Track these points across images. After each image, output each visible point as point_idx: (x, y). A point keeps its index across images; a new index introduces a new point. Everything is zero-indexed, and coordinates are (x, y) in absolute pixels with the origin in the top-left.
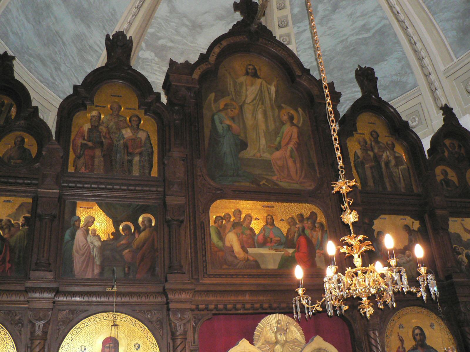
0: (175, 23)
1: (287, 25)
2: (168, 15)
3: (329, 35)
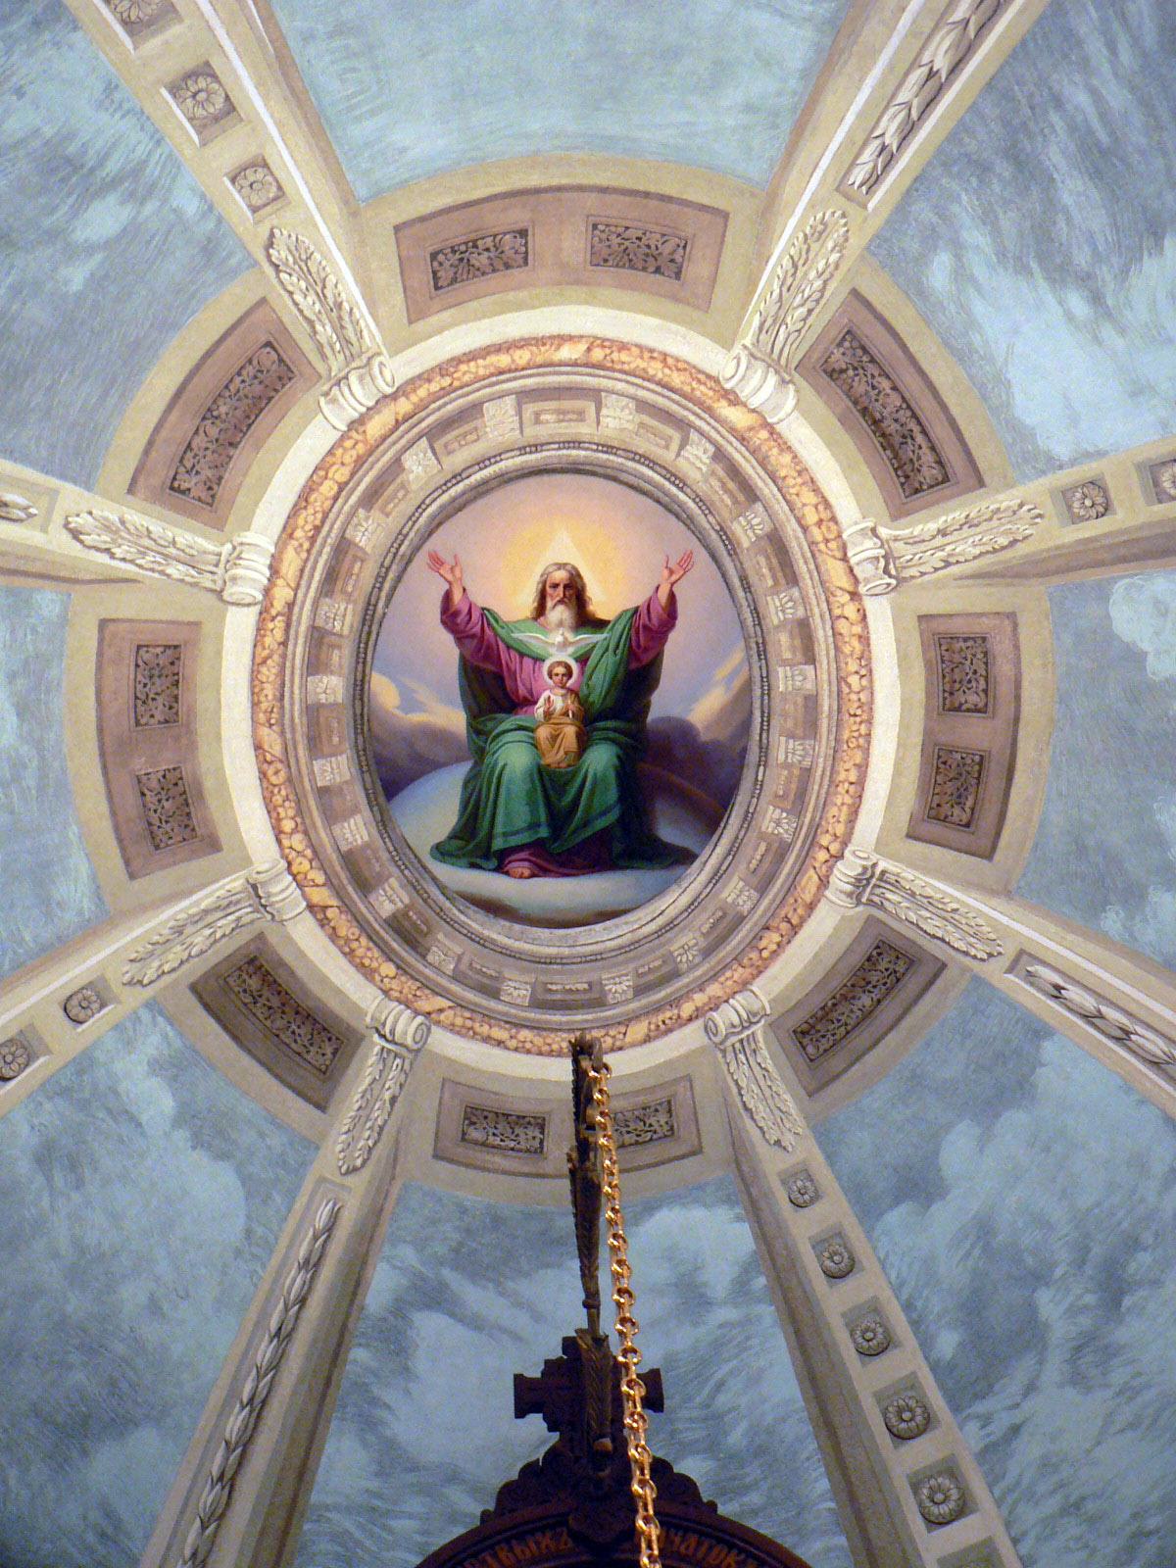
0: (411, 1516)
1: (929, 1422)
2: (374, 1485)
3: (1132, 1426)
